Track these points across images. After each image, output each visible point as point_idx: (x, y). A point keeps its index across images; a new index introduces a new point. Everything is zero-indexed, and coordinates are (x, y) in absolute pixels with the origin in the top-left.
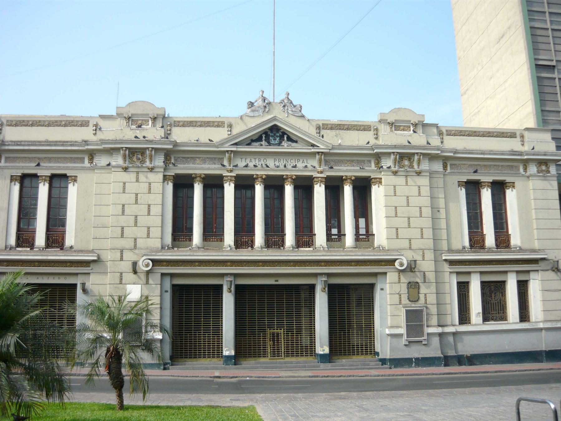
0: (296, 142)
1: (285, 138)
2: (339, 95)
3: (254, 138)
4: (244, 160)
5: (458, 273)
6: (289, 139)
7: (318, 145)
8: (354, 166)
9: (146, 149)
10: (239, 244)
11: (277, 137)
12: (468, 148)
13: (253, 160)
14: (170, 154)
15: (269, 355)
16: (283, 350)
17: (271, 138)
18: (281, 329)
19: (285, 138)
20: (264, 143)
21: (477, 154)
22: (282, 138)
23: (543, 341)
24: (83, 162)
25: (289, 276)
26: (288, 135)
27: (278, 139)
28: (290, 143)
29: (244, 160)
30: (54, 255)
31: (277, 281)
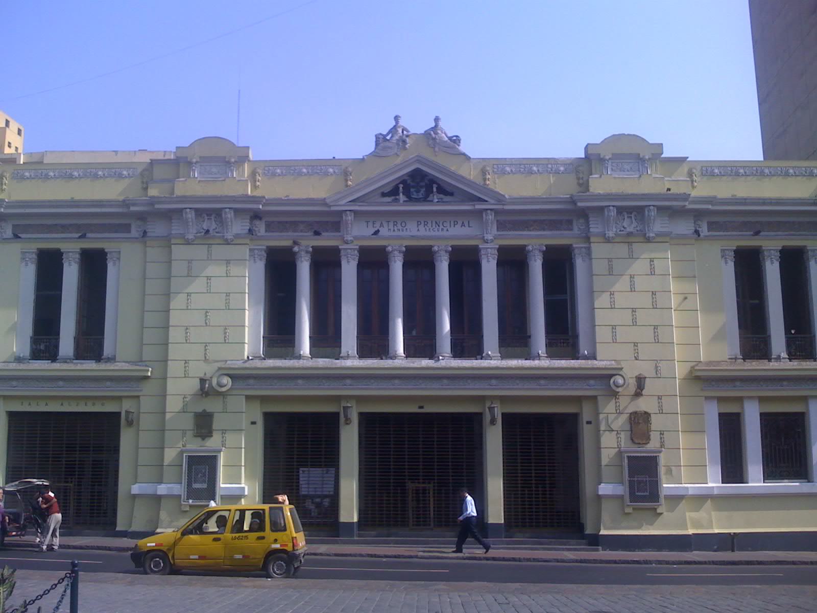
0: (451, 194)
1: (435, 190)
2: (520, 124)
3: (387, 190)
4: (370, 224)
5: (720, 400)
6: (442, 190)
7: (486, 198)
8: (544, 230)
9: (221, 209)
10: (412, 351)
11: (422, 187)
12: (291, 197)
13: (385, 224)
14: (256, 214)
15: (432, 523)
16: (432, 515)
17: (412, 190)
18: (429, 483)
19: (435, 190)
20: (402, 197)
21: (111, 206)
22: (429, 191)
23: (359, 538)
24: (129, 232)
25: (441, 400)
26: (439, 185)
27: (423, 190)
28: (441, 196)
29: (370, 224)
30: (89, 367)
31: (421, 407)
